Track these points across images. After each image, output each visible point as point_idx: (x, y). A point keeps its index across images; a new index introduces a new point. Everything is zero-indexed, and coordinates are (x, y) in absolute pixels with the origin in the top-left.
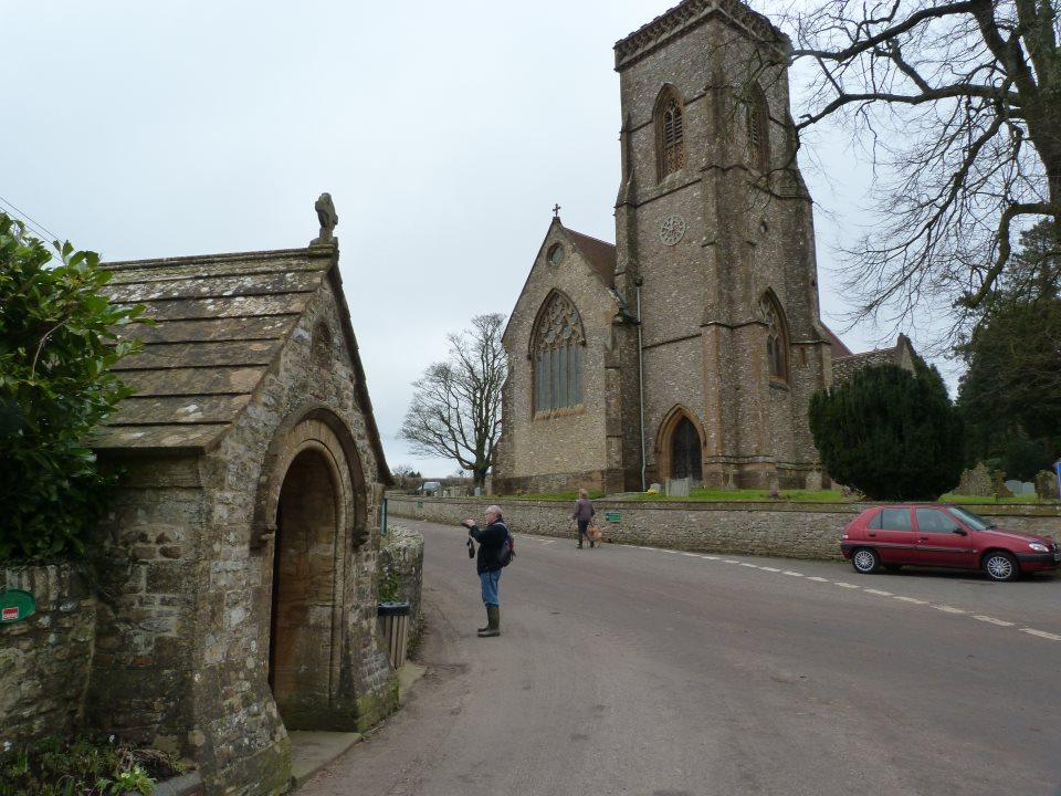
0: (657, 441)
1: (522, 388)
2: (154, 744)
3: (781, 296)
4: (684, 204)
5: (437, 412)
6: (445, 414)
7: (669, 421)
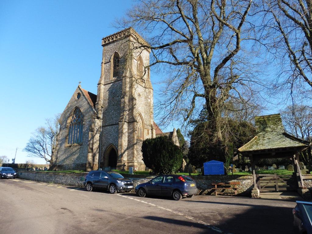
0: (104, 155)
1: (176, 141)
2: (283, 131)
3: (143, 115)
4: (117, 86)
5: (38, 142)
6: (42, 144)
7: (109, 148)
